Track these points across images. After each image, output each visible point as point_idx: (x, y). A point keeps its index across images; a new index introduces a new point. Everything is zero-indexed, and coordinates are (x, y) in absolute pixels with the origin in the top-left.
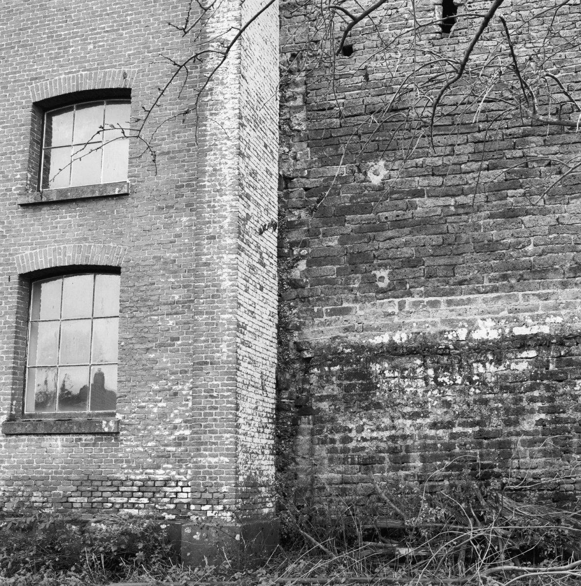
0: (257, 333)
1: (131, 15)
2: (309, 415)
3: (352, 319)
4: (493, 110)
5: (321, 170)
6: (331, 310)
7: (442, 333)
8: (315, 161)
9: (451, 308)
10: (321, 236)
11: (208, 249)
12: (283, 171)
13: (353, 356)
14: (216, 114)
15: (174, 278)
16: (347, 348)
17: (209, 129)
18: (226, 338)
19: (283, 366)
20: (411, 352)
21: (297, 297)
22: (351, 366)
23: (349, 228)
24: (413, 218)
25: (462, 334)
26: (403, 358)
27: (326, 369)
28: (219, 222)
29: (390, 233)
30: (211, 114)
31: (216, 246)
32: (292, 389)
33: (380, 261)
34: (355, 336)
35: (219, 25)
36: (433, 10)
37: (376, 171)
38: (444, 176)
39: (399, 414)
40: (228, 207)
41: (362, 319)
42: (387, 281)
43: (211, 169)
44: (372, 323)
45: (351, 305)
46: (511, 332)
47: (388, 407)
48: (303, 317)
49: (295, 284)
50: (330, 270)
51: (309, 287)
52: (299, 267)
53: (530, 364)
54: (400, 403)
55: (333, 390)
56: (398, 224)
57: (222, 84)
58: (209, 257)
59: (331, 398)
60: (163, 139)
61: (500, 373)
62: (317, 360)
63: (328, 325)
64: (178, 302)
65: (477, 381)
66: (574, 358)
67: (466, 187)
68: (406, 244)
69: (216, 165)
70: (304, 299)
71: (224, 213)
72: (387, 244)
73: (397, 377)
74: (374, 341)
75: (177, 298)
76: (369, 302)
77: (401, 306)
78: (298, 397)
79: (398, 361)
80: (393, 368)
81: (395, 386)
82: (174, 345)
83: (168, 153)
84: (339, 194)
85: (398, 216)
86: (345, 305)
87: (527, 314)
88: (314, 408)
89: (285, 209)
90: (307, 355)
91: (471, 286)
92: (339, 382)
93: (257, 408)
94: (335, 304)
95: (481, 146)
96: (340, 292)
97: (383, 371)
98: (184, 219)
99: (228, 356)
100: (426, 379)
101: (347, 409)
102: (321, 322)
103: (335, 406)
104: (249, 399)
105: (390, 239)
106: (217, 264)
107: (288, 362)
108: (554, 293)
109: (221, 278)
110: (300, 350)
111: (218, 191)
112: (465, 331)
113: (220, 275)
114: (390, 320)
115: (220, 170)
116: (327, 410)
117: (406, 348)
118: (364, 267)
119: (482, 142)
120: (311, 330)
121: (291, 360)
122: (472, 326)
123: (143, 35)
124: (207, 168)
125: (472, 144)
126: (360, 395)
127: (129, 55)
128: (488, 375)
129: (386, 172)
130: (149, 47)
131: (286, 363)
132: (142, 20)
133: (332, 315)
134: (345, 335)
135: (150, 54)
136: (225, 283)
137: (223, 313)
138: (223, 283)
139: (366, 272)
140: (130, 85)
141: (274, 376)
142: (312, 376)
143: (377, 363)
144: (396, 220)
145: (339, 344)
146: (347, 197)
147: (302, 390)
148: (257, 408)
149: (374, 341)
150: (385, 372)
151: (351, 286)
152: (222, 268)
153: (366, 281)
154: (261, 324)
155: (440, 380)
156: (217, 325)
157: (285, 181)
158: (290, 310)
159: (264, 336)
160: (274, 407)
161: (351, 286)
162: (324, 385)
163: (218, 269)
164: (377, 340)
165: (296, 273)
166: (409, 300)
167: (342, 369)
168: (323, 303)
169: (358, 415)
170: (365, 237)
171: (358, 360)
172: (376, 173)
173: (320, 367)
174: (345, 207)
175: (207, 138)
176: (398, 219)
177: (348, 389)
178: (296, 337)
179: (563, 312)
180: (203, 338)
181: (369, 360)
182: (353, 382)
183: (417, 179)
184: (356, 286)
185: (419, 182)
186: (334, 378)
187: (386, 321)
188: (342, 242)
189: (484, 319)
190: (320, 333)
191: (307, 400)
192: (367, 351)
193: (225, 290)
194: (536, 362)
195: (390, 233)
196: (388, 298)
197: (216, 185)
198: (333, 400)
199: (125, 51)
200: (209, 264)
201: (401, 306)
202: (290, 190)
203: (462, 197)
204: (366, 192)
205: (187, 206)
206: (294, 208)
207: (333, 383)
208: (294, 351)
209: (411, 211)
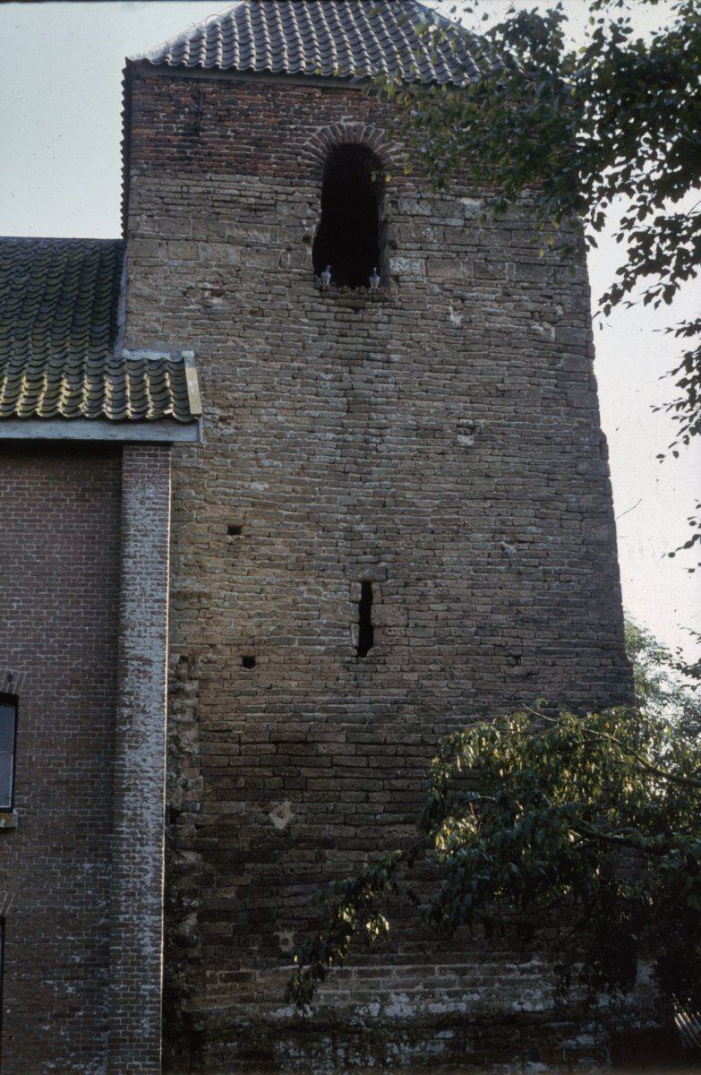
1: (18, 601)
4: (411, 755)
5: (216, 804)
6: (227, 975)
7: (353, 1008)
9: (363, 980)
10: (214, 885)
11: (127, 907)
14: (136, 748)
15: (73, 935)
17: (127, 764)
18: (147, 1012)
20: (320, 1029)
25: (374, 1008)
27: (222, 1044)
28: (139, 877)
29: (296, 889)
30: (130, 747)
35: (141, 640)
36: (349, 628)
37: (280, 813)
38: (357, 826)
40: (150, 860)
41: (261, 988)
43: (130, 813)
45: (250, 971)
46: (427, 1008)
50: (224, 927)
53: (446, 1045)
56: (304, 879)
57: (144, 712)
58: (127, 916)
60: (61, 765)
61: (415, 1055)
64: (79, 965)
65: (390, 1063)
66: (492, 1040)
67: (381, 841)
69: (135, 808)
71: (146, 867)
75: (78, 959)
82: (73, 1016)
83: (67, 782)
87: (443, 990)
91: (384, 955)
94: (231, 969)
95: (398, 796)
96: (237, 954)
98: (87, 866)
99: (151, 1034)
100: (334, 1060)
105: (296, 895)
106: (138, 925)
108: (471, 968)
109: (142, 942)
111: (138, 839)
112: (377, 1006)
115: (141, 815)
119: (399, 791)
122: (385, 999)
123: (34, 630)
124: (125, 811)
125: (388, 793)
127: (16, 652)
128: (403, 1057)
129: (292, 816)
130: (42, 646)
132: (32, 610)
135: (43, 656)
137: (145, 982)
140: (17, 691)
155: (351, 1061)
157: (173, 815)
163: (139, 931)
172: (280, 815)
175: (126, 775)
179: (481, 989)
180: (120, 1011)
183: (327, 827)
185: (330, 831)
189: (397, 994)
194: (451, 1044)
195: (296, 889)
197: (135, 833)
199: (10, 647)
203: (376, 852)
205: (91, 850)
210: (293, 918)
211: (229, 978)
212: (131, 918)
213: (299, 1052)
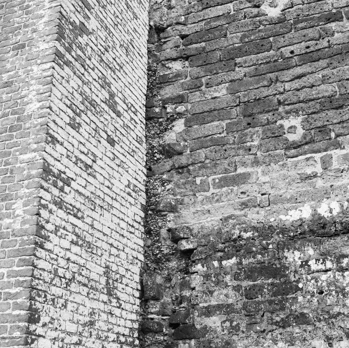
0: (97, 201)
2: (190, 339)
3: (251, 189)
6: (221, 180)
8: (194, 5)
12: (155, 21)
13: (257, 242)
16: (246, 231)
19: (153, 266)
21: (173, 168)
22: (254, 257)
23: (239, 72)
24: (329, 47)
26: (338, 239)
27: (216, 264)
31: (24, 57)
32: (167, 299)
33: (288, 108)
34: (258, 213)
39: (341, 332)
41: (266, 188)
42: (300, 132)
44: (282, 191)
45: (249, 170)
47: (320, 321)
48: (181, 193)
49: (169, 152)
50: (215, 127)
51: (188, 152)
52: (174, 128)
54: (339, 314)
55: (226, 296)
56: (309, 57)
59: (226, 309)
62: (201, 253)
63: (217, 201)
68: (324, 80)
70: (181, 169)
71: (41, 12)
72: (296, 84)
73: (330, 270)
74: (288, 217)
76: (276, 163)
77: (326, 164)
78: (174, 311)
79: (328, 244)
80: (324, 256)
81: (329, 285)
84: (225, 36)
85: (308, 47)
86: (241, 170)
88: (198, 327)
89: (157, 64)
90: (185, 245)
92: (236, 283)
93: (92, 323)
97: (307, 262)
99: (24, 223)
101: (250, 325)
102: (207, 197)
103: (231, 322)
104: (70, 306)
105: (299, 77)
107: (160, 259)
110: (176, 240)
113: (25, 96)
114: (310, 185)
116: (219, 329)
117: (342, 223)
118: (264, 118)
120: (193, 210)
121: (165, 255)
126: (271, 302)
131: (157, 261)
133: (223, 187)
134: (243, 212)
136: (30, 106)
138: (28, 107)
139: (268, 123)
141: (137, 278)
142: (193, 276)
143: (295, 249)
144: (306, 53)
145: (234, 226)
146: (237, 37)
147: (180, 300)
148: (92, 323)
149: (288, 217)
150: (310, 263)
151: (248, 144)
152: (28, 84)
153: (270, 135)
154: (107, 190)
156: (11, 173)
157: (157, 31)
158: (163, 185)
159: (115, 211)
160: (136, 326)
161: (248, 144)
162: (211, 289)
164: (292, 216)
165: (170, 137)
166: (336, 153)
167: (240, 263)
168: (209, 171)
169: (269, 336)
170: (264, 79)
171: (265, 248)
173: (205, 261)
174: (235, 49)
176: (308, 50)
177: (250, 294)
178: (171, 221)
181: (281, 247)
182: (259, 282)
184: (256, 143)
186: (228, 278)
187: (304, 187)
188: (232, 92)
190: (203, 214)
191: (187, 315)
192: (278, 234)
193: (30, 117)
195: (299, 70)
196: (305, 153)
198: (228, 313)
200: (12, 82)
201: (326, 164)
202: (163, 40)
204: (262, 27)
206: (167, 60)
207: (227, 286)
208: (169, 242)
209: (327, 39)
210: (300, 102)
211: (224, 182)
212: (17, 75)
213: (324, 262)
